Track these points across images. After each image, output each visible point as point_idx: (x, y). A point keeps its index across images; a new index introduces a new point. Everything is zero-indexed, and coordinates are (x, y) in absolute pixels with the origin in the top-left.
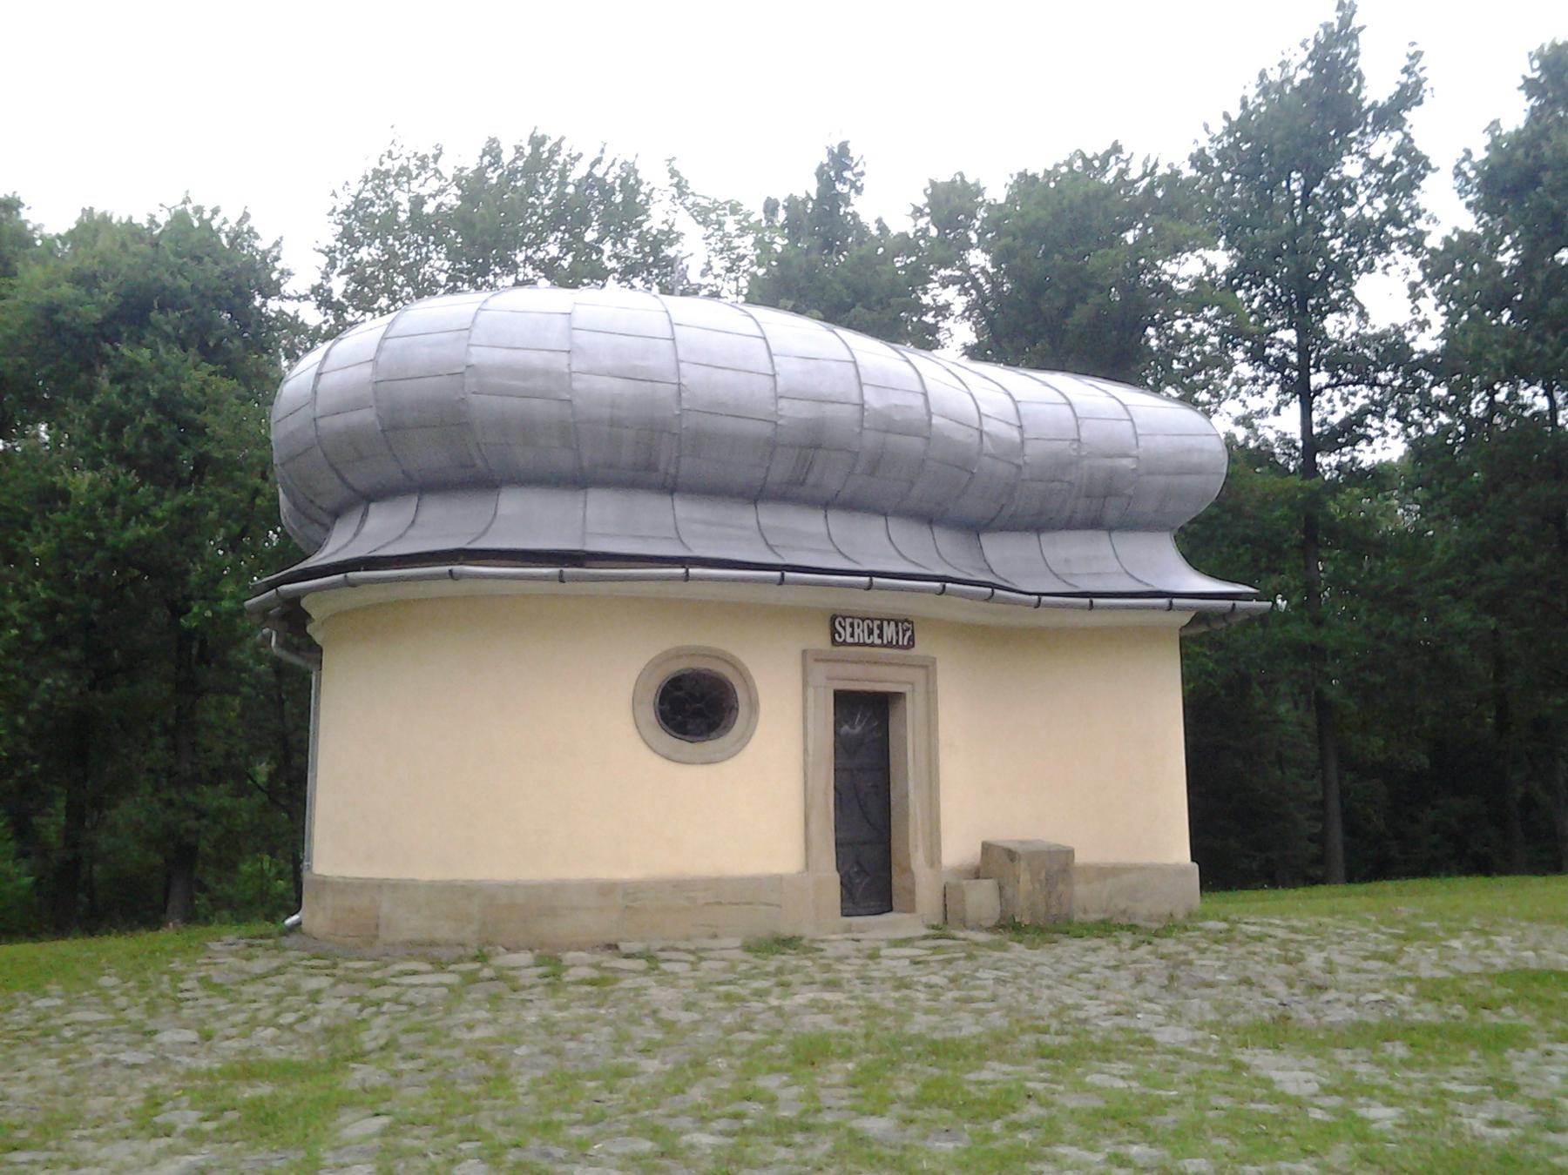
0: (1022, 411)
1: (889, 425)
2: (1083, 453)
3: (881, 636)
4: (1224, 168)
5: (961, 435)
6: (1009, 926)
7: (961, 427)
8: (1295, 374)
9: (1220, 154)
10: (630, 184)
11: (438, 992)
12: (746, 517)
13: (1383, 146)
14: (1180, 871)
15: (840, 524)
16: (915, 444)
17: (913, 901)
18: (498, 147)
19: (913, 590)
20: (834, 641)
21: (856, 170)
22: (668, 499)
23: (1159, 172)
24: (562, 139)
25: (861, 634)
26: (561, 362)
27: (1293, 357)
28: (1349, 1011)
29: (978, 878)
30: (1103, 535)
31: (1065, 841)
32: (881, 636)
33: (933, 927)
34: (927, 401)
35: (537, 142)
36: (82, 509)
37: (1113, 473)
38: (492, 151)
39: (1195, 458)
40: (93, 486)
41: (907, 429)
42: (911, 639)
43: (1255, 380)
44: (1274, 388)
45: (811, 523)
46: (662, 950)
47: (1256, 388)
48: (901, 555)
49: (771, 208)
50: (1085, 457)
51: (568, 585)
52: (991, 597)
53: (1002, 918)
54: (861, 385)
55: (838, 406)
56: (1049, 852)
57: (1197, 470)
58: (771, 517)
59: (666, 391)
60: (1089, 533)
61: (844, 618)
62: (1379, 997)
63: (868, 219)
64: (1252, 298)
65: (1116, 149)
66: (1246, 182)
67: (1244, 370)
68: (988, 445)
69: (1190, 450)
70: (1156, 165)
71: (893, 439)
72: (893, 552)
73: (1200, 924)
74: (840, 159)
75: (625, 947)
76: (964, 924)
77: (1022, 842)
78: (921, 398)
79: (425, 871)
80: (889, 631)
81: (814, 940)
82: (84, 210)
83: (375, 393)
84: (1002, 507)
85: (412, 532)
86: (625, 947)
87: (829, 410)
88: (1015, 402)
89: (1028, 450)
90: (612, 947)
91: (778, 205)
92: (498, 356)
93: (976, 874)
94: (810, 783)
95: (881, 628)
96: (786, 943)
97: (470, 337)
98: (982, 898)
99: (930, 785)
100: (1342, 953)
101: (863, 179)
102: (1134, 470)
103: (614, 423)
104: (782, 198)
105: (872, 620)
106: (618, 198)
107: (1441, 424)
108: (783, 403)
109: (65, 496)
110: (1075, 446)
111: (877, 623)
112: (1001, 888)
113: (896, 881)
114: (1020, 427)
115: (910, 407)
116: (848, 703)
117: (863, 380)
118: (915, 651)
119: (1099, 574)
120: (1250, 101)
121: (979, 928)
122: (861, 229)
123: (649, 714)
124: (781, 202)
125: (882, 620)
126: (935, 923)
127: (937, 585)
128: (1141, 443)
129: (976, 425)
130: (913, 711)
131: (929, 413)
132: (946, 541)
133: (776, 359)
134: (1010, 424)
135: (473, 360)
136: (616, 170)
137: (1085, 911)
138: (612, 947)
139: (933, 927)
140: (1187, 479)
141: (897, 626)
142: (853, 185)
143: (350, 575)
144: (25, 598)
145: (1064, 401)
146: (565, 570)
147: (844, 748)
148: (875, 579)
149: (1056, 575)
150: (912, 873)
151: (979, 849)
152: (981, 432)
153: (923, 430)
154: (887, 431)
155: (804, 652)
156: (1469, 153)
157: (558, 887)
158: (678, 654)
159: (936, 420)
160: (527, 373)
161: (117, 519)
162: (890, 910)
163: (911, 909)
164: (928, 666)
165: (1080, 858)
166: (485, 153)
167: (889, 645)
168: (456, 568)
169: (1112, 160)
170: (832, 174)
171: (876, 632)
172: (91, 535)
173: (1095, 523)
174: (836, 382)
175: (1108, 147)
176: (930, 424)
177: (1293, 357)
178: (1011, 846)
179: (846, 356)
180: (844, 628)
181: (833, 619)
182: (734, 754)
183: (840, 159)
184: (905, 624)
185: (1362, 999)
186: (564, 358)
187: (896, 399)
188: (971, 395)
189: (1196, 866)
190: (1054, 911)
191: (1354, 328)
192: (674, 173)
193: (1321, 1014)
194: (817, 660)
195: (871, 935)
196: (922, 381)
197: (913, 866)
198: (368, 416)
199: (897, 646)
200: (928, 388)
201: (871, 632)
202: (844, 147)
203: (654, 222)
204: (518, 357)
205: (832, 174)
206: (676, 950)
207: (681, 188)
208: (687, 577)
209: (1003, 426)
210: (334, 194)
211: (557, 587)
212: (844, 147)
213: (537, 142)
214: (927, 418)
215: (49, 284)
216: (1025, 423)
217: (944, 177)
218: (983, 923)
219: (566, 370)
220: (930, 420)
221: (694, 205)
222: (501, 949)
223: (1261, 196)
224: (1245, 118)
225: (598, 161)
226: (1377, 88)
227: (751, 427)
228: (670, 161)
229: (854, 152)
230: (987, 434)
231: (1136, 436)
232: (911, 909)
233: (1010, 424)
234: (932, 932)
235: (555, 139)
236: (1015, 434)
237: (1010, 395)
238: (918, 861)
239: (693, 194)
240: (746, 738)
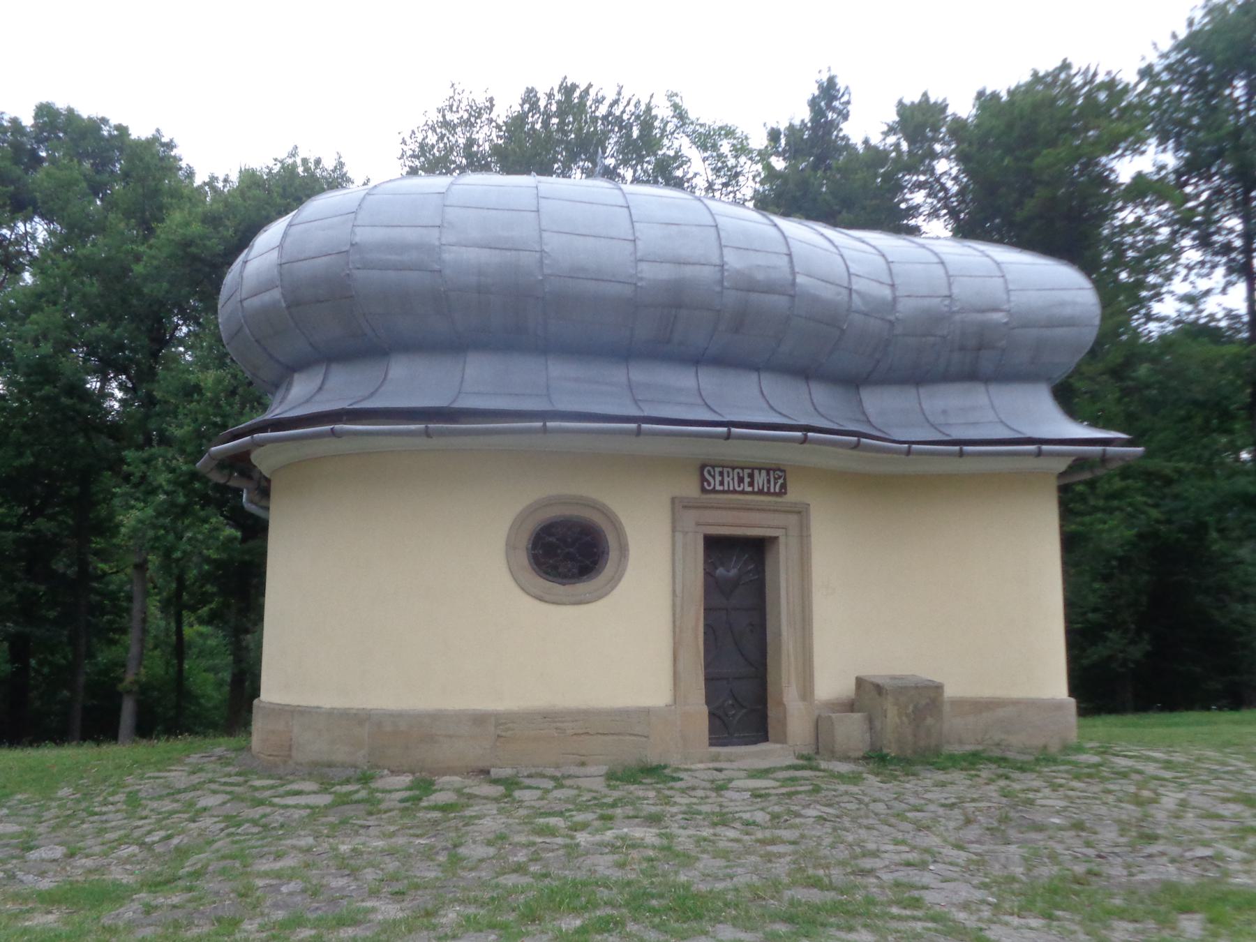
0: (894, 271)
1: (750, 285)
2: (955, 309)
3: (751, 484)
4: (1172, 81)
5: (827, 293)
6: (877, 759)
7: (829, 286)
8: (1240, 257)
9: (1168, 68)
10: (647, 121)
11: (297, 814)
12: (618, 374)
14: (1057, 706)
15: (709, 380)
16: (781, 301)
17: (785, 733)
18: (535, 96)
19: (690, 435)
20: (704, 490)
21: (845, 99)
23: (1099, 80)
24: (590, 86)
26: (433, 237)
28: (1172, 868)
29: (852, 711)
30: (980, 388)
31: (937, 679)
32: (751, 484)
33: (801, 757)
34: (791, 261)
35: (568, 90)
36: (211, 400)
38: (530, 98)
39: (1068, 311)
40: (219, 381)
41: (769, 288)
42: (784, 486)
43: (1202, 263)
44: (1220, 271)
45: (683, 379)
46: (530, 776)
47: (1205, 271)
48: (771, 407)
49: (774, 135)
50: (958, 312)
52: (805, 440)
53: (872, 750)
54: (721, 247)
55: (698, 268)
56: (917, 687)
57: (1070, 322)
58: (640, 374)
59: (527, 259)
60: (966, 386)
61: (713, 467)
62: (1207, 852)
63: (857, 140)
64: (1198, 191)
66: (1194, 92)
67: (1193, 256)
68: (857, 301)
69: (1062, 304)
70: (1095, 75)
71: (754, 296)
72: (765, 405)
73: (1073, 758)
74: (828, 92)
75: (495, 773)
76: (833, 755)
77: (893, 678)
78: (786, 259)
79: (328, 700)
80: (760, 479)
81: (677, 770)
83: (281, 274)
84: (878, 361)
85: (318, 398)
86: (495, 773)
87: (688, 271)
88: (888, 263)
89: (900, 307)
91: (780, 133)
92: (380, 234)
93: (850, 706)
94: (678, 623)
95: (751, 476)
96: (652, 772)
97: (355, 219)
98: (851, 731)
100: (1203, 794)
101: (850, 107)
102: (1006, 324)
104: (782, 127)
105: (743, 469)
106: (635, 133)
108: (643, 266)
109: (197, 388)
110: (947, 302)
111: (747, 471)
112: (870, 720)
113: (772, 712)
114: (893, 286)
115: (775, 268)
116: (716, 546)
117: (723, 243)
119: (975, 424)
120: (1196, 21)
121: (846, 759)
122: (849, 147)
123: (523, 558)
124: (782, 130)
125: (753, 469)
126: (805, 752)
127: (799, 434)
128: (1012, 298)
129: (846, 284)
131: (794, 273)
132: (821, 394)
133: (637, 225)
134: (881, 283)
135: (357, 239)
136: (631, 108)
137: (961, 742)
139: (801, 757)
141: (768, 474)
142: (840, 113)
144: (173, 471)
145: (936, 260)
146: (431, 426)
147: (713, 585)
148: (733, 430)
149: (932, 425)
150: (784, 705)
151: (852, 684)
152: (850, 290)
153: (789, 289)
155: (673, 500)
157: (436, 717)
158: (549, 503)
159: (800, 279)
160: (404, 247)
161: (237, 407)
162: (765, 738)
163: (782, 740)
164: (801, 512)
165: (950, 692)
166: (524, 102)
167: (761, 492)
168: (338, 427)
170: (823, 104)
171: (747, 480)
172: (218, 420)
173: (972, 375)
174: (771, 265)
175: (1058, 64)
176: (794, 283)
177: (1238, 243)
178: (879, 681)
179: (621, 202)
180: (714, 477)
181: (703, 467)
182: (606, 594)
183: (828, 92)
184: (776, 471)
185: (1188, 854)
186: (436, 232)
187: (760, 259)
188: (842, 256)
189: (1073, 700)
192: (676, 107)
193: (1134, 870)
194: (684, 507)
195: (735, 765)
196: (787, 244)
197: (785, 699)
198: (276, 294)
199: (769, 493)
200: (793, 250)
201: (741, 480)
202: (832, 82)
203: (666, 151)
204: (396, 234)
205: (823, 104)
206: (544, 776)
207: (681, 115)
209: (875, 284)
210: (404, 142)
211: (422, 442)
212: (832, 82)
213: (568, 90)
214: (790, 277)
215: (187, 224)
216: (897, 281)
217: (912, 97)
218: (850, 754)
219: (437, 243)
220: (794, 279)
221: (694, 132)
222: (386, 772)
223: (1207, 103)
224: (1192, 37)
225: (616, 102)
228: (671, 96)
229: (841, 84)
230: (858, 293)
231: (1008, 291)
232: (782, 740)
233: (881, 283)
234: (801, 762)
235: (583, 87)
236: (886, 292)
237: (883, 256)
239: (692, 123)
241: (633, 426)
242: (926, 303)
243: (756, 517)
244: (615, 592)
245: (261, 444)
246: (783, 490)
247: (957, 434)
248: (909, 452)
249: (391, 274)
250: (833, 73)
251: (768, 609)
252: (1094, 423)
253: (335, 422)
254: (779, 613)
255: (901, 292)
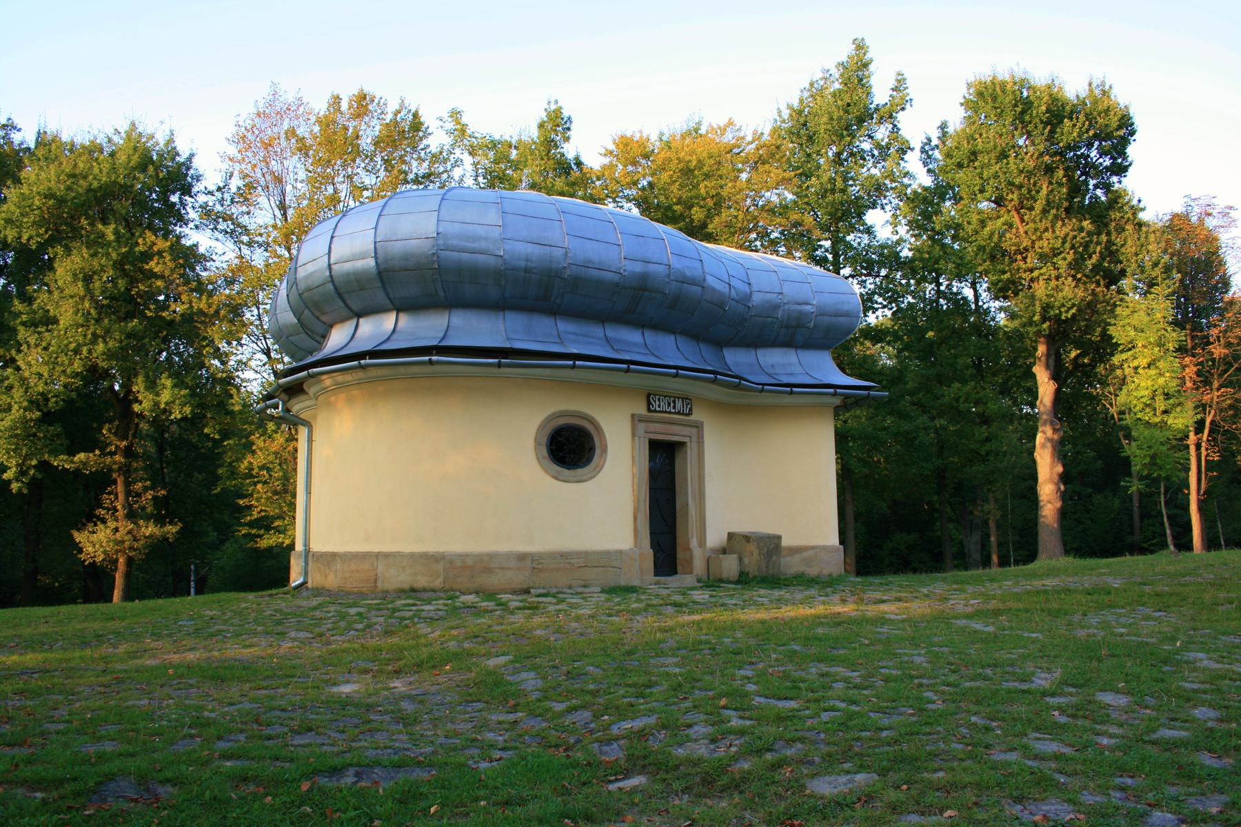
1: (684, 280)
3: (674, 408)
10: (417, 125)
12: (597, 331)
13: (882, 133)
14: (837, 550)
15: (651, 337)
20: (649, 410)
22: (552, 319)
25: (664, 407)
27: (830, 257)
30: (792, 351)
31: (777, 533)
32: (674, 408)
37: (801, 315)
39: (846, 307)
41: (693, 282)
42: (691, 410)
45: (634, 336)
51: (503, 370)
65: (731, 123)
69: (843, 302)
80: (679, 404)
82: (962, 104)
87: (652, 267)
90: (527, 592)
93: (724, 551)
95: (674, 402)
98: (730, 566)
99: (700, 498)
103: (527, 270)
107: (909, 302)
113: (680, 556)
118: (691, 418)
130: (691, 451)
132: (706, 350)
138: (527, 592)
140: (841, 319)
143: (362, 362)
151: (726, 536)
154: (683, 282)
155: (633, 416)
156: (929, 140)
158: (562, 414)
159: (709, 278)
160: (476, 239)
162: (676, 573)
164: (698, 426)
165: (785, 543)
167: (679, 413)
168: (435, 358)
169: (728, 130)
176: (704, 280)
177: (830, 257)
181: (648, 396)
184: (686, 399)
189: (842, 547)
190: (771, 572)
191: (866, 242)
199: (683, 414)
208: (574, 367)
211: (496, 370)
212: (558, 112)
222: (458, 593)
226: (881, 95)
227: (609, 276)
232: (691, 572)
236: (746, 288)
238: (694, 543)
240: (599, 469)
241: (625, 366)
242: (768, 296)
243: (675, 428)
244: (601, 474)
245: (310, 376)
246: (690, 414)
247: (786, 380)
248: (762, 391)
249: (465, 256)
250: (559, 105)
251: (677, 489)
252: (860, 377)
253: (431, 354)
254: (687, 492)
255: (755, 288)
